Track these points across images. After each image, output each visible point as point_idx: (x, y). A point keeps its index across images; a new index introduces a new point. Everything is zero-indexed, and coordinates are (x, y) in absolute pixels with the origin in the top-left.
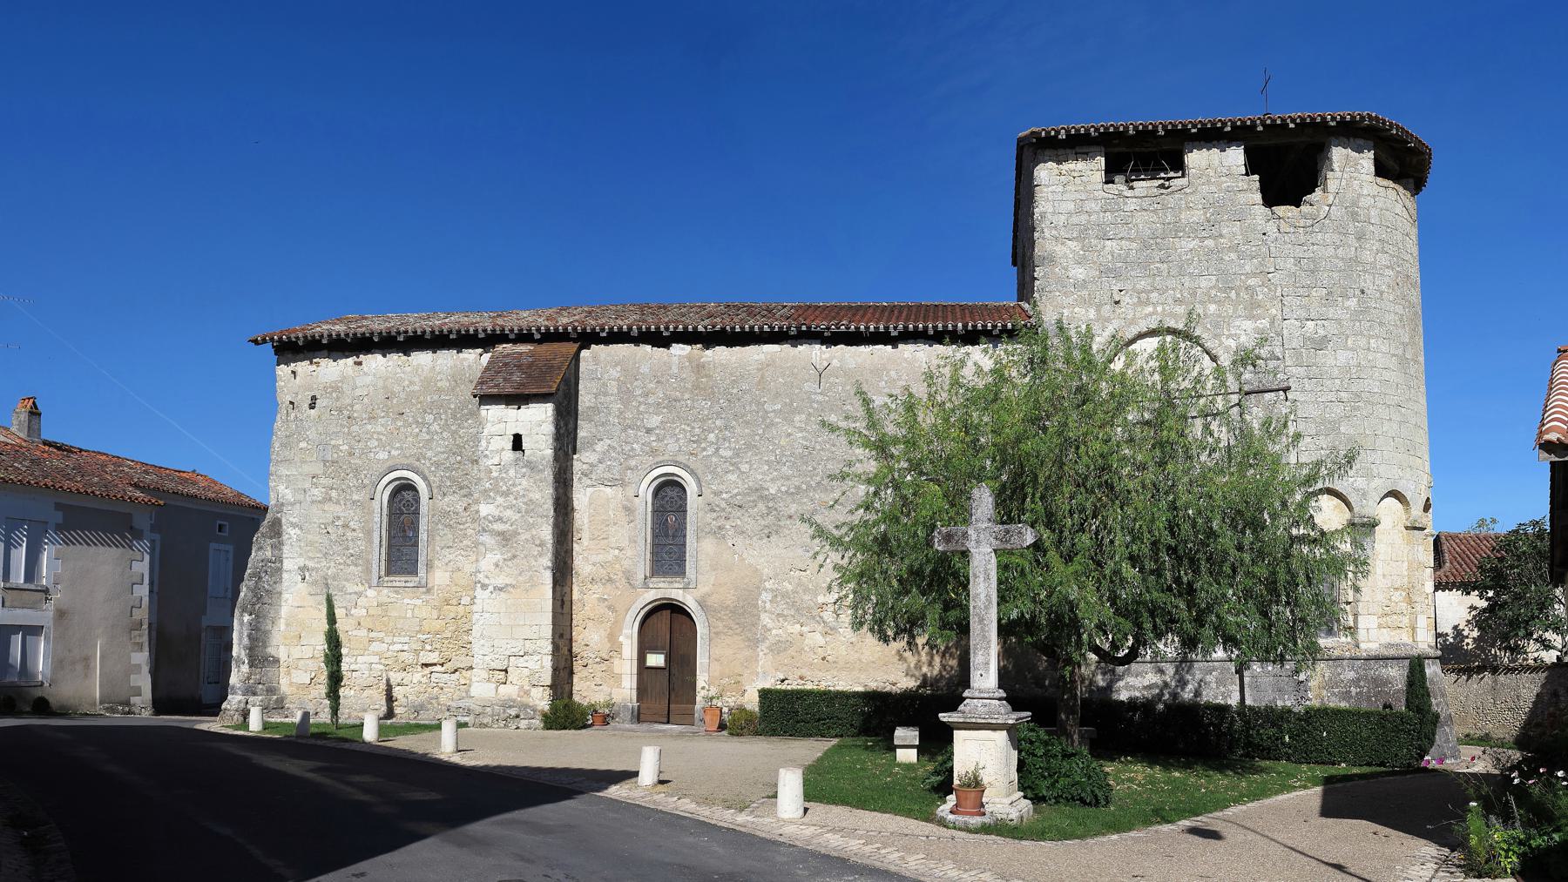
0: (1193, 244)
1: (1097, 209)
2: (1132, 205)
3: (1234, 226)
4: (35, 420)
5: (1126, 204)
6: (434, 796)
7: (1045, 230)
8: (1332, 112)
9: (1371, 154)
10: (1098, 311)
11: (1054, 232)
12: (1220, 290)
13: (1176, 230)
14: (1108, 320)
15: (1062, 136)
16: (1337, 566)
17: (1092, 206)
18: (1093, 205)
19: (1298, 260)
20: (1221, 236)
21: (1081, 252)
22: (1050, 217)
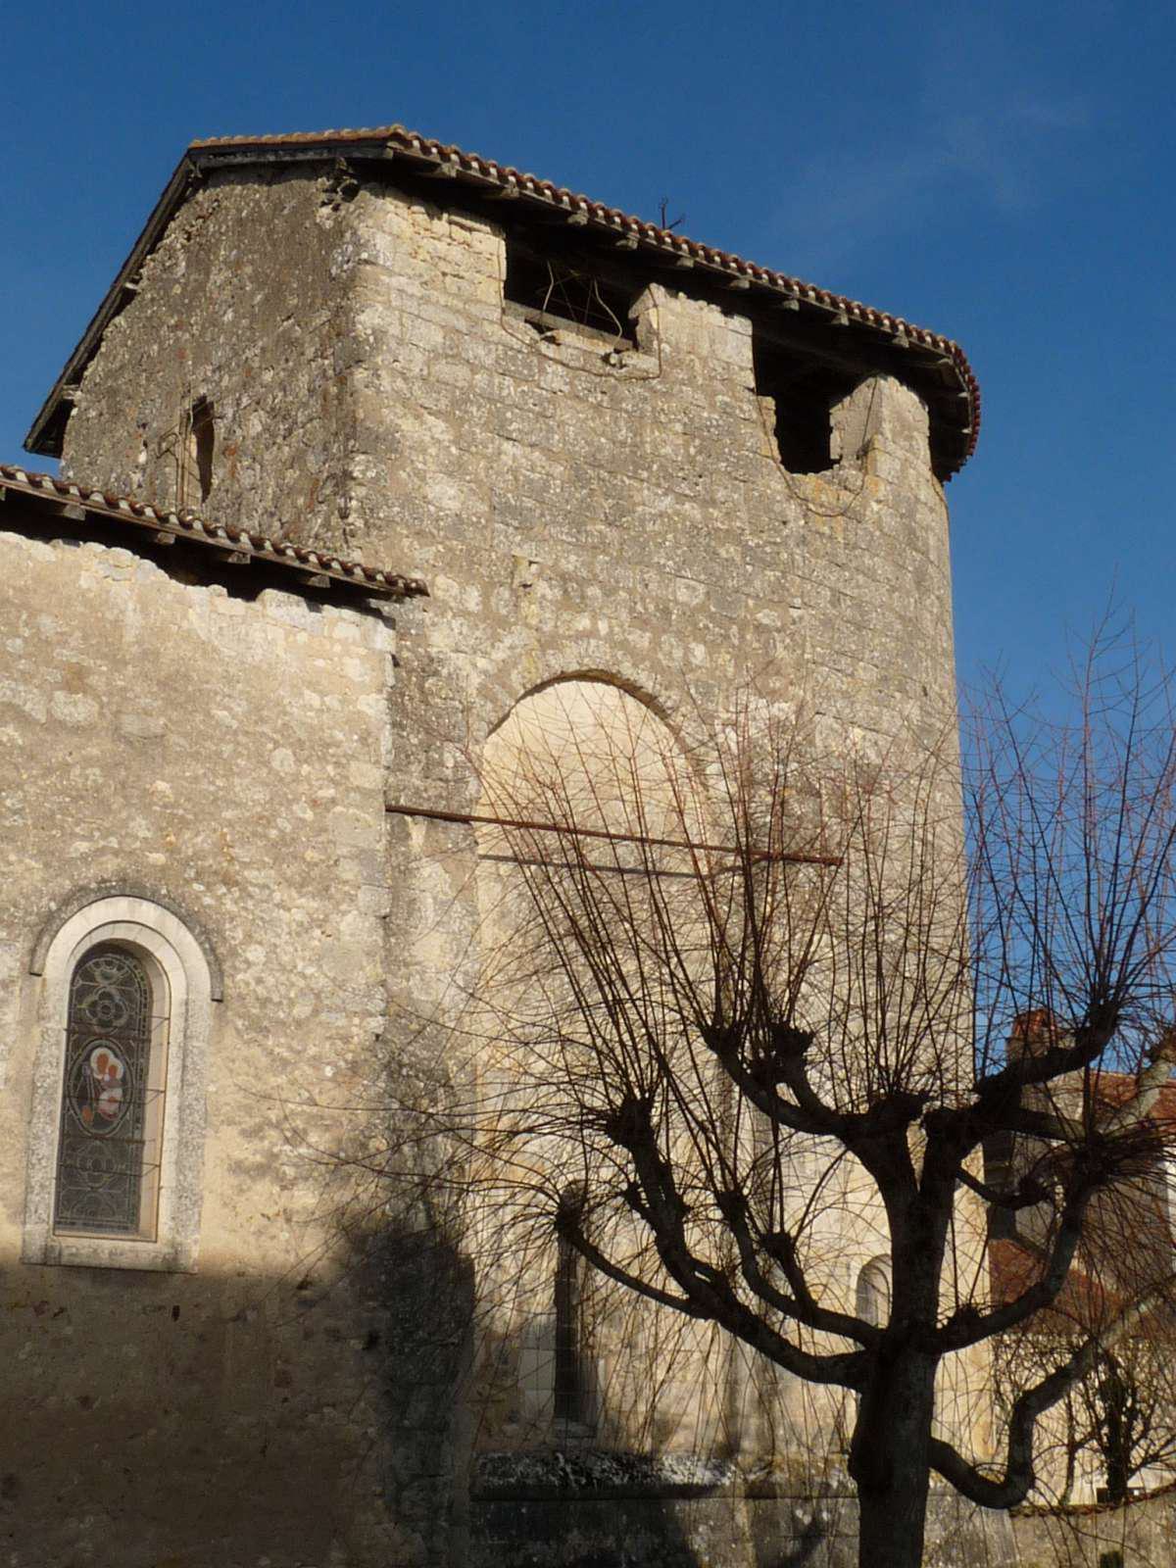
0: (667, 503)
1: (489, 361)
2: (555, 378)
3: (736, 489)
4: (638, 694)
5: (542, 371)
6: (917, 1165)
7: (383, 373)
8: (904, 323)
9: (658, 291)
10: (486, 596)
11: (400, 383)
12: (711, 617)
13: (635, 460)
14: (503, 623)
15: (450, 170)
16: (175, 1259)
17: (477, 351)
18: (481, 352)
19: (837, 597)
20: (713, 503)
21: (453, 450)
22: (393, 345)
